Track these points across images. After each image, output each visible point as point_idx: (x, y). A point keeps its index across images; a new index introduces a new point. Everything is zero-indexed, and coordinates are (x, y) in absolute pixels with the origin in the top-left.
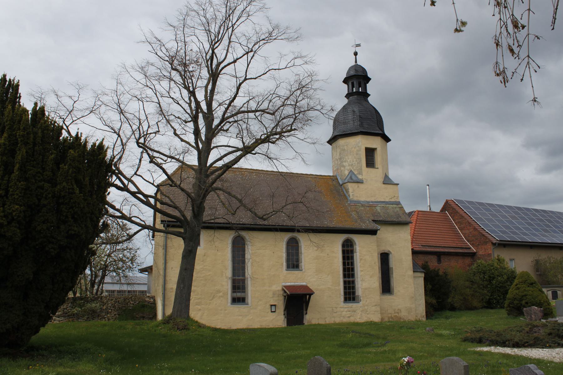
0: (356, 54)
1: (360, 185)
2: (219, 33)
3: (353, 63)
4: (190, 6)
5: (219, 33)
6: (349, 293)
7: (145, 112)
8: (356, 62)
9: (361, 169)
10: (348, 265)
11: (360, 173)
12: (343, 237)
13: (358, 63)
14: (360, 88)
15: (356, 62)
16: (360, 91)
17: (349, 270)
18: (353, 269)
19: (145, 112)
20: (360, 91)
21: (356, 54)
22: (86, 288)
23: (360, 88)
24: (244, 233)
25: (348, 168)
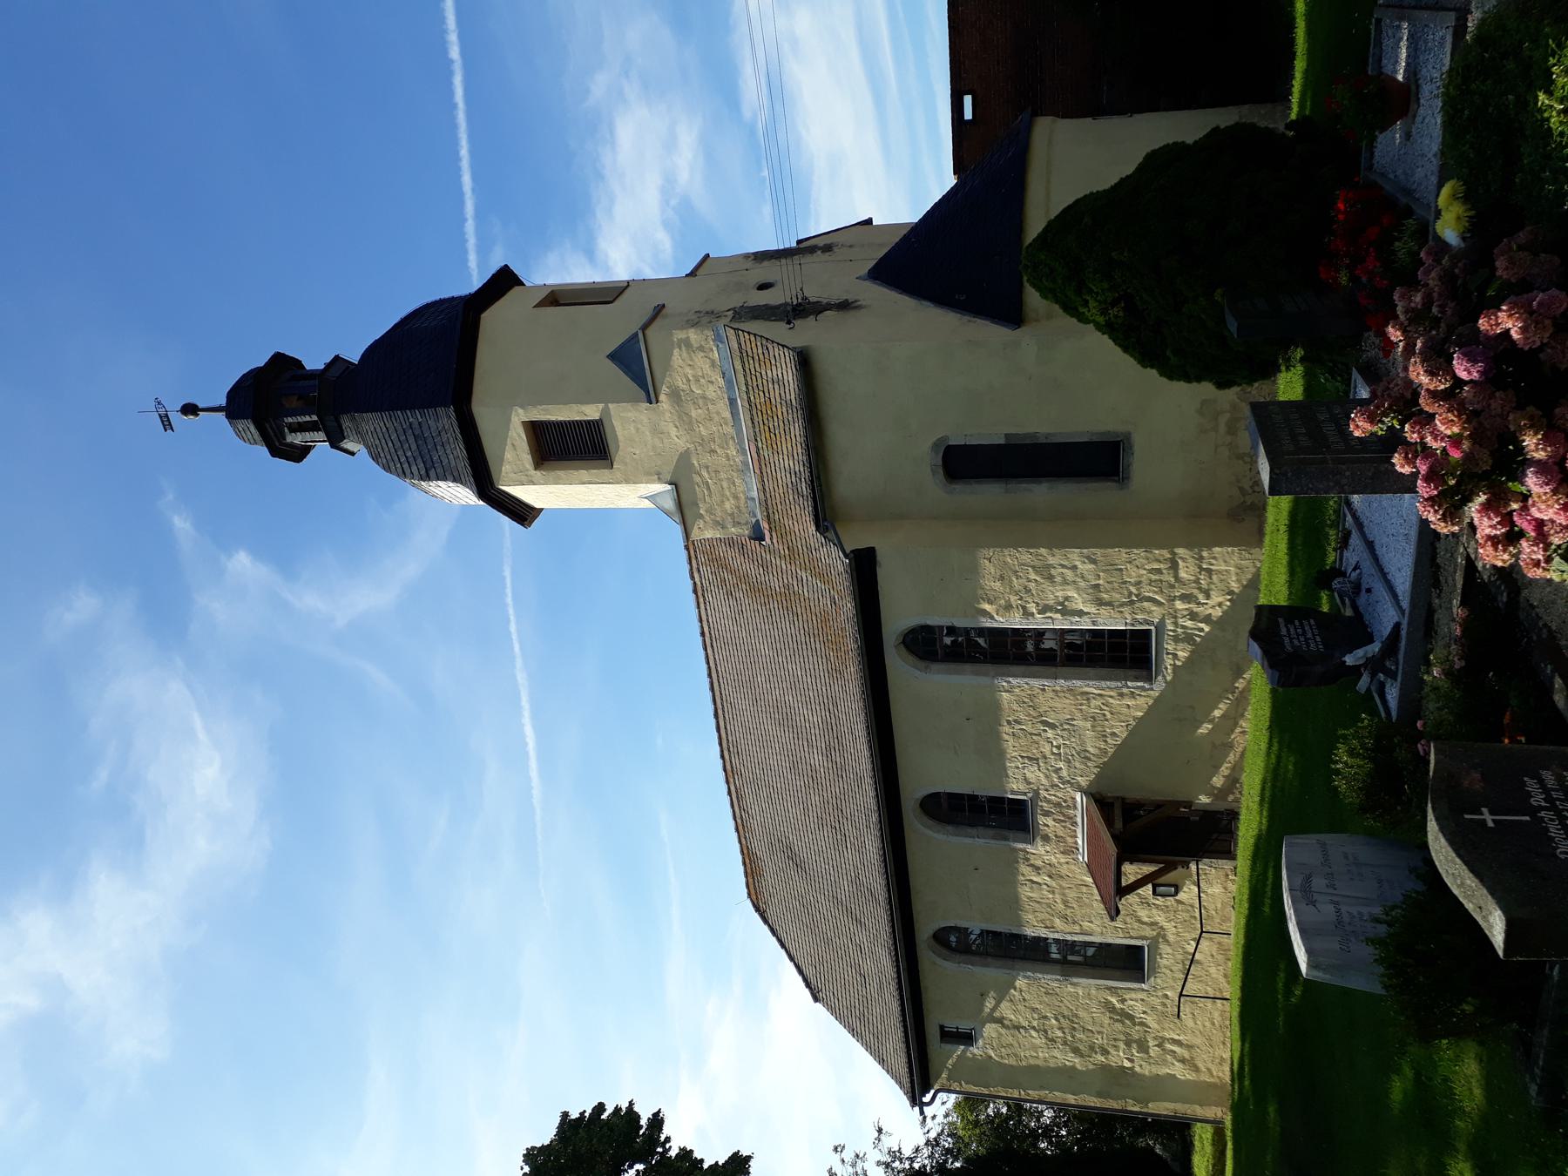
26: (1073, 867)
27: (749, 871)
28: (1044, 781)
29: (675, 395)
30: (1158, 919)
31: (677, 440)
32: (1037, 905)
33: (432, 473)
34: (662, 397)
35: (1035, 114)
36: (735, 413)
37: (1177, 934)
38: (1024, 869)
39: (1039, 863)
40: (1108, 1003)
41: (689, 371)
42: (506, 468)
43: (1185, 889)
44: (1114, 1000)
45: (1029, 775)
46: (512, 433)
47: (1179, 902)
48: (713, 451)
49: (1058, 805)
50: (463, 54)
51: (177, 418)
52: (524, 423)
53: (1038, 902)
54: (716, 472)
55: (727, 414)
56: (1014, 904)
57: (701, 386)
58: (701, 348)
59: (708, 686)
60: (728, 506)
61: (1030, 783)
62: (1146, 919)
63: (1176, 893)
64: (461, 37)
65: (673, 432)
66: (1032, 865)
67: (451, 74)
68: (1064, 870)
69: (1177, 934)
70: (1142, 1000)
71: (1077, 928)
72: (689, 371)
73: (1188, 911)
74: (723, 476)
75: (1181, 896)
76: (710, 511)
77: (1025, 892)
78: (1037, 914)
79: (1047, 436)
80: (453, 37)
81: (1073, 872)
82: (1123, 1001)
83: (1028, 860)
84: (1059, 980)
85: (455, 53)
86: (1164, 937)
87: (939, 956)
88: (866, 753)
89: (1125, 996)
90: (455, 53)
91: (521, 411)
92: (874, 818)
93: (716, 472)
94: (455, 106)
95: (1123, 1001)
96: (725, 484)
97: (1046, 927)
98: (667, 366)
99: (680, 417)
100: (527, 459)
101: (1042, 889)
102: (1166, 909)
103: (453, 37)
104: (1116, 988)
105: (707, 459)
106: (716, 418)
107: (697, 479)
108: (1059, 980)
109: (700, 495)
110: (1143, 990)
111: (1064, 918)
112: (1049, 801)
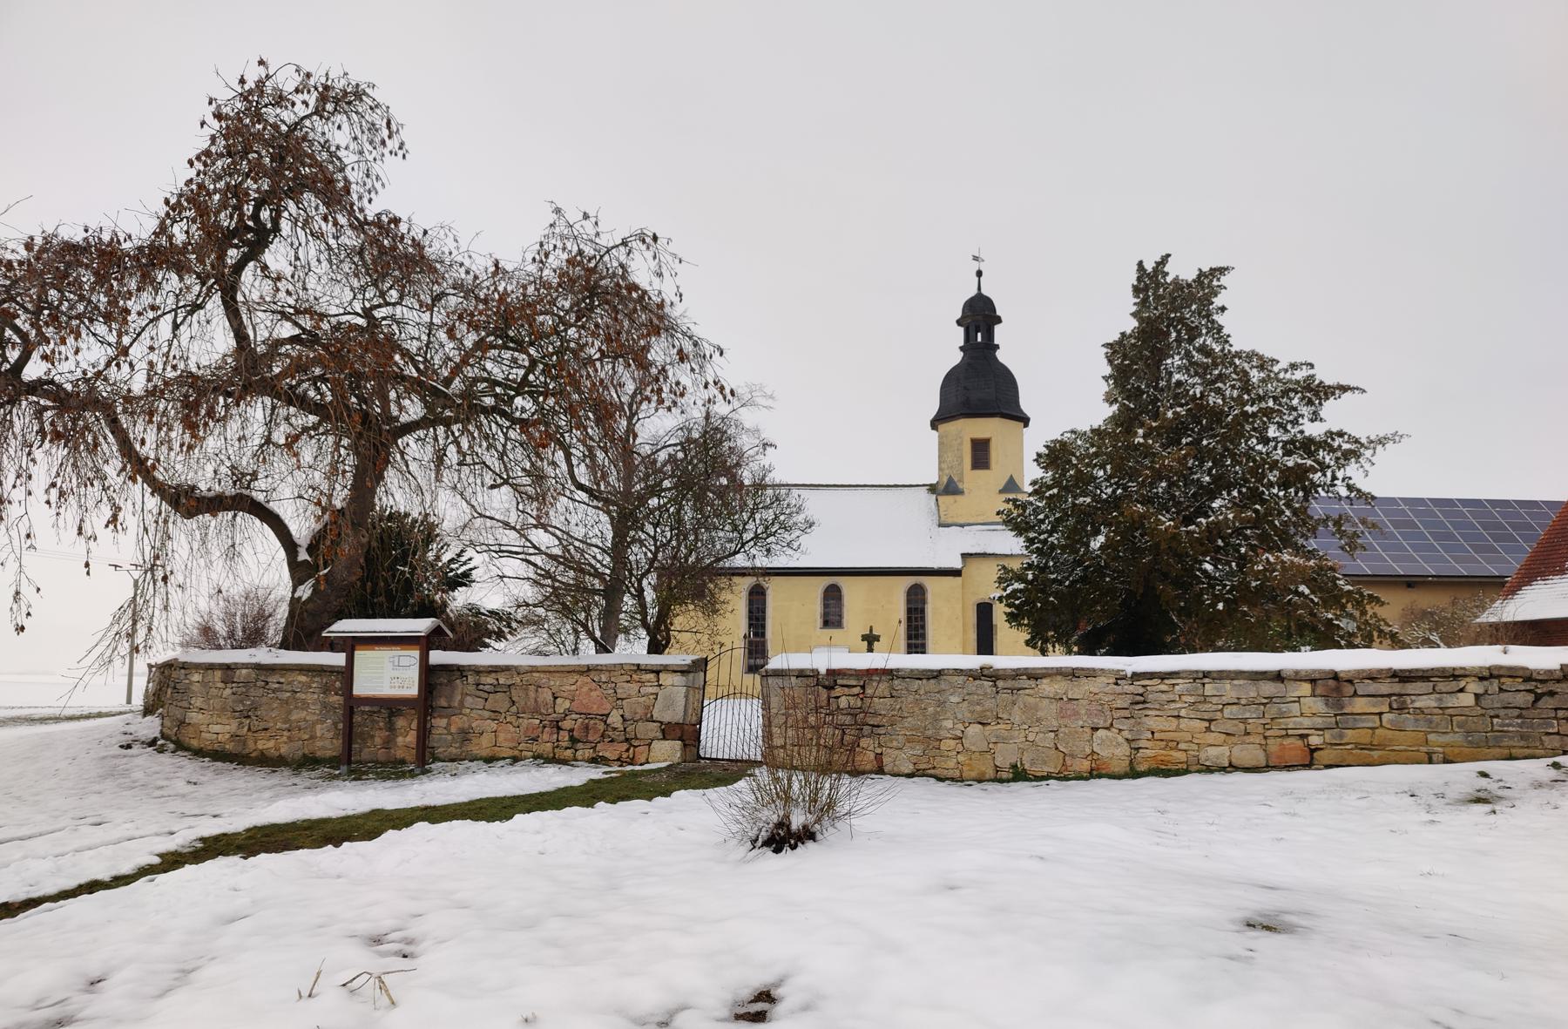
0: (979, 274)
1: (958, 497)
2: (757, 798)
3: (974, 292)
4: (179, 704)
5: (757, 798)
6: (917, 637)
7: (92, 887)
8: (979, 288)
9: (962, 474)
10: (916, 618)
11: (961, 480)
12: (910, 581)
13: (985, 292)
14: (979, 334)
15: (979, 288)
16: (979, 339)
17: (916, 628)
18: (923, 627)
19: (92, 887)
20: (979, 339)
21: (979, 274)
22: (1518, 717)
23: (979, 334)
25: (947, 472)
51: (975, 266)
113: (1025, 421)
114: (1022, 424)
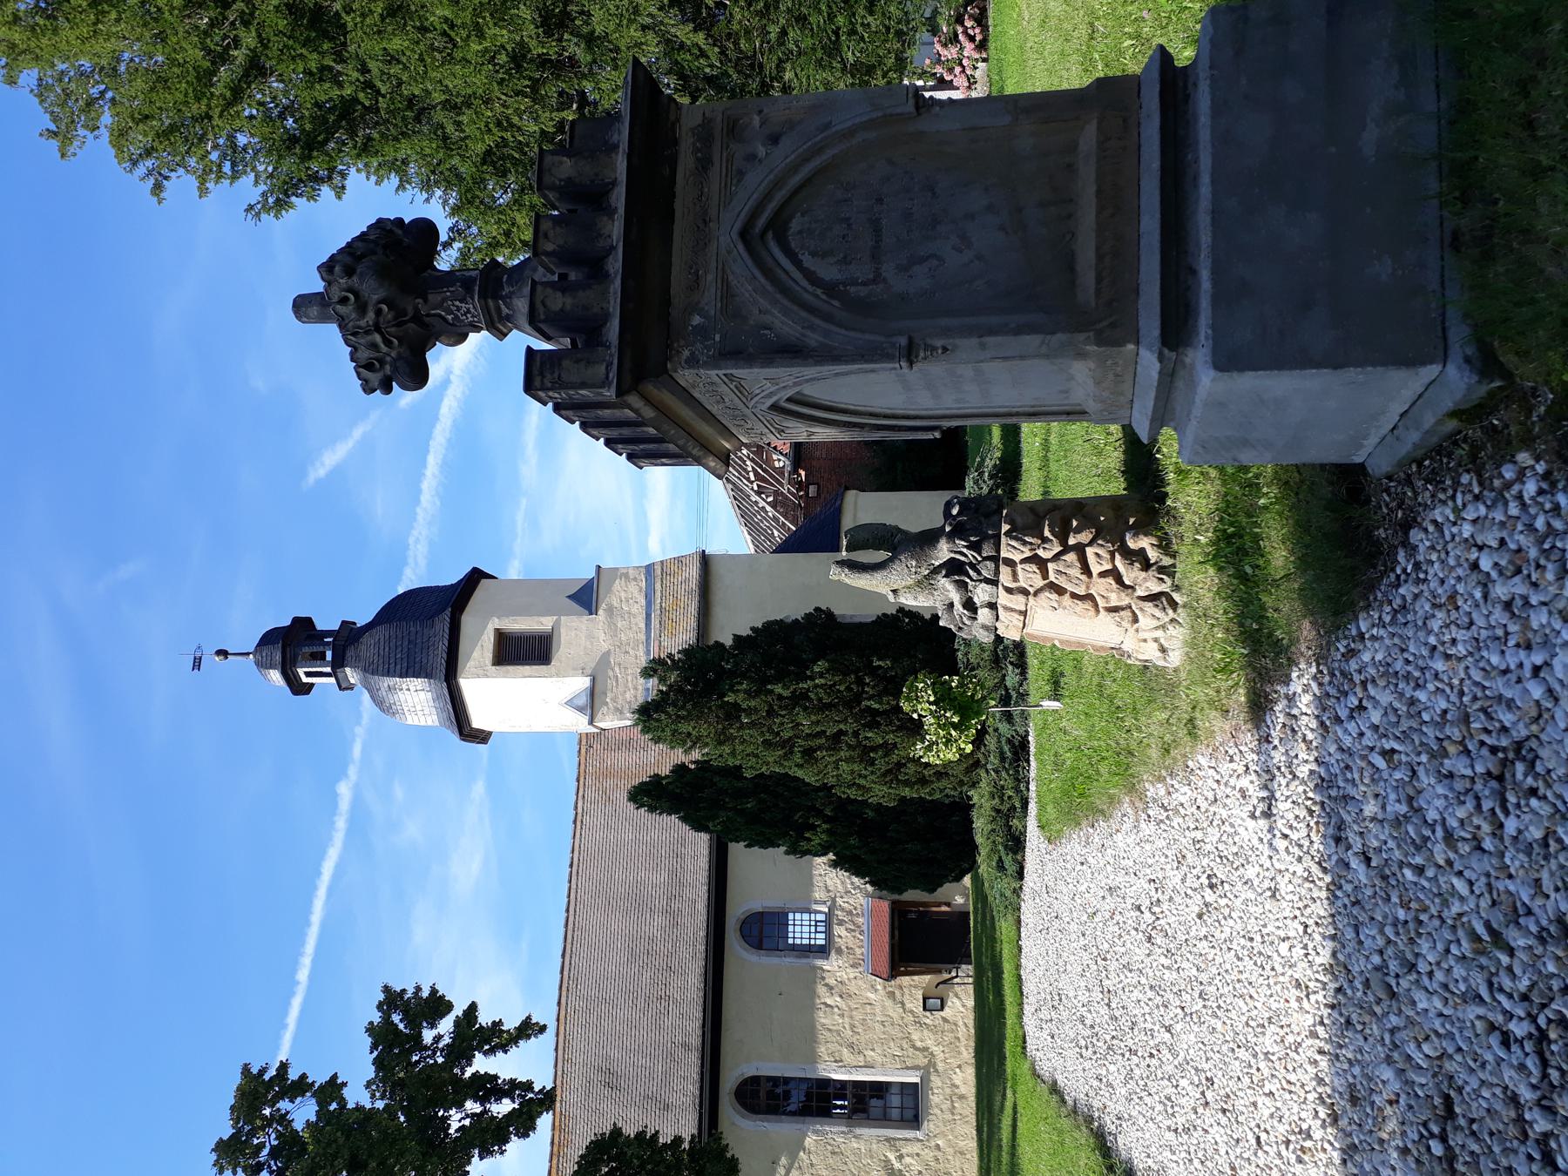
24: (730, 1080)
26: (860, 983)
27: (557, 1124)
28: (840, 888)
29: (610, 610)
30: (929, 1043)
31: (603, 643)
32: (829, 1034)
33: (411, 671)
34: (601, 612)
35: (847, 488)
36: (648, 625)
37: (945, 1061)
38: (821, 990)
39: (832, 982)
40: (887, 1161)
41: (623, 595)
42: (471, 664)
43: (949, 1003)
44: (892, 1156)
45: (829, 883)
46: (485, 637)
47: (945, 1020)
48: (627, 652)
49: (850, 913)
50: (311, 977)
51: (211, 661)
52: (497, 630)
53: (830, 1030)
54: (626, 668)
55: (643, 625)
56: (809, 1036)
57: (629, 605)
58: (635, 579)
59: (562, 937)
60: (628, 696)
61: (829, 891)
62: (919, 1044)
63: (942, 1009)
64: (314, 962)
65: (602, 636)
66: (826, 985)
67: (292, 994)
68: (853, 988)
69: (945, 1061)
70: (918, 1155)
71: (861, 1058)
72: (623, 595)
73: (952, 1031)
74: (630, 671)
75: (947, 1012)
76: (614, 700)
77: (823, 1019)
78: (829, 1045)
79: (852, 616)
80: (307, 961)
81: (859, 988)
82: (901, 1157)
83: (823, 978)
84: (843, 1132)
85: (303, 975)
86: (934, 1065)
87: (738, 1113)
88: (706, 852)
89: (904, 1151)
90: (303, 975)
91: (496, 620)
92: (702, 933)
93: (626, 668)
94: (285, 1026)
95: (901, 1157)
96: (630, 678)
97: (836, 1061)
98: (609, 590)
99: (609, 626)
100: (489, 655)
101: (833, 1014)
102: (933, 1029)
103: (307, 961)
104: (894, 1139)
105: (621, 658)
106: (634, 628)
107: (611, 673)
108: (843, 1132)
109: (609, 687)
110: (919, 1140)
111: (851, 1046)
112: (843, 910)
113: (476, 577)
114: (484, 582)
